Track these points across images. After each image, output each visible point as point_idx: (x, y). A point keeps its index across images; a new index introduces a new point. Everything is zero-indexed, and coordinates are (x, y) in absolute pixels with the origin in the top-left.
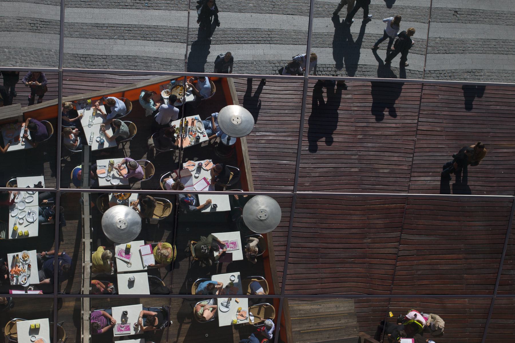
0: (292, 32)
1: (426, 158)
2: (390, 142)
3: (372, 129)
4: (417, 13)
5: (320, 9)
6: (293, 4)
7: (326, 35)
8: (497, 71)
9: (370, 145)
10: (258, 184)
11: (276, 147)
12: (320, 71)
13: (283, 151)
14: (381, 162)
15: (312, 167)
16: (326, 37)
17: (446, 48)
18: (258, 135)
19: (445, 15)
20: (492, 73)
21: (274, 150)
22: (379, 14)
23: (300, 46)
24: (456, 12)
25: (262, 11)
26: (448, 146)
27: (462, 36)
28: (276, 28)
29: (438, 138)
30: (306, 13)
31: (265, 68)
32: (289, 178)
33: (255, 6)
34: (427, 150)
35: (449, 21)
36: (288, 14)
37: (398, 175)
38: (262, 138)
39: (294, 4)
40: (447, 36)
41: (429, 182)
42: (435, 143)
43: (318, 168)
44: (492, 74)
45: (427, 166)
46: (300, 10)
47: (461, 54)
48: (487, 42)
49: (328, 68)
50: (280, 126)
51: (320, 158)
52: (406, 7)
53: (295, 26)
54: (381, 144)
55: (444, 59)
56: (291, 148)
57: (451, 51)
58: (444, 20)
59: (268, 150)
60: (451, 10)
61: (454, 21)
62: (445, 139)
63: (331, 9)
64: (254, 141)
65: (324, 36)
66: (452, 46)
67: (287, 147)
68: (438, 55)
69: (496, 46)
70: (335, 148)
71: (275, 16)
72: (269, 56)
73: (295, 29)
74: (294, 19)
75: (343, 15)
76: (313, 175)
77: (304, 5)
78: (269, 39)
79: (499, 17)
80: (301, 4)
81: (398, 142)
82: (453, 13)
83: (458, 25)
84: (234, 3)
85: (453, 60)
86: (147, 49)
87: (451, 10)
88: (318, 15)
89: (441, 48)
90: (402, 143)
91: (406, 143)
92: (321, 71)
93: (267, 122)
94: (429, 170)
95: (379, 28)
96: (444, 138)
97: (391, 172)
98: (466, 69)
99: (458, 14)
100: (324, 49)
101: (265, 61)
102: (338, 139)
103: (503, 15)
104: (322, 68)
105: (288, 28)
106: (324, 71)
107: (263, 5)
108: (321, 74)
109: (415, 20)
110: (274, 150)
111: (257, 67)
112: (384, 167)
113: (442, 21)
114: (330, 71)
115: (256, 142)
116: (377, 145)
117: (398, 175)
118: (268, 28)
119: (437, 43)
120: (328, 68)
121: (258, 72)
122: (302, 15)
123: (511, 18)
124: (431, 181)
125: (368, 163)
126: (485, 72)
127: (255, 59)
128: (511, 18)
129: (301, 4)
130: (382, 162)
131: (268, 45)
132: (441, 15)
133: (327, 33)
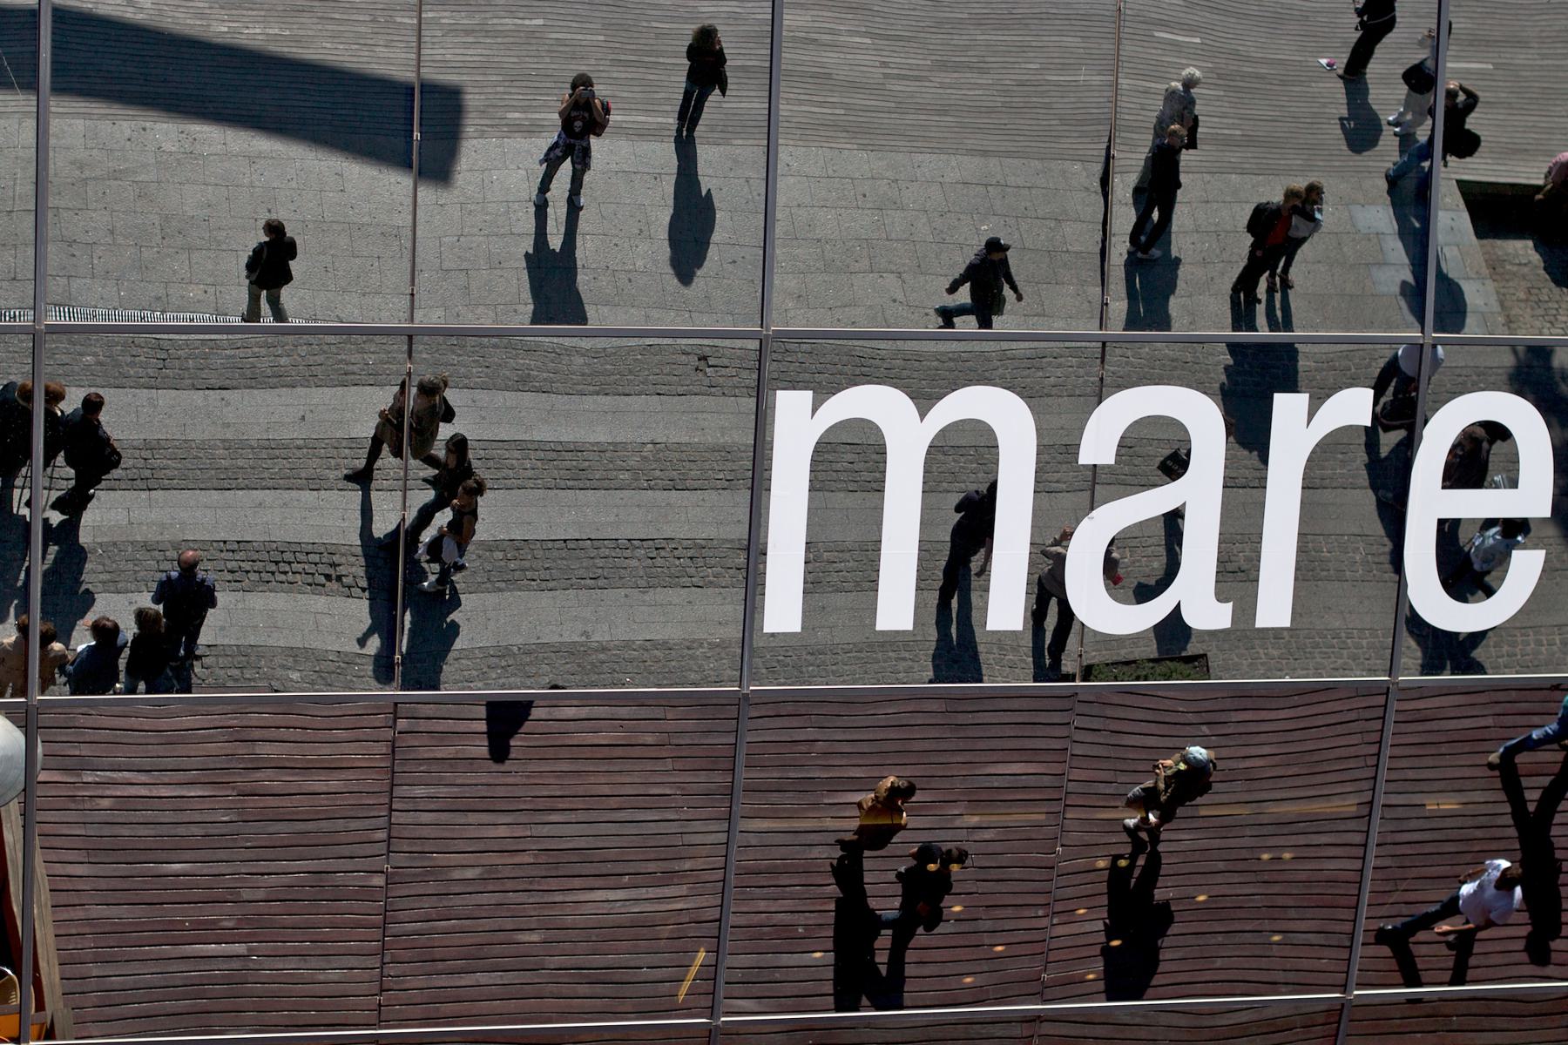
0: (219, 448)
1: (612, 828)
2: (484, 781)
3: (425, 739)
4: (608, 367)
5: (283, 361)
6: (228, 352)
7: (299, 448)
8: (857, 544)
9: (420, 791)
10: (87, 945)
11: (151, 820)
12: (284, 562)
13: (173, 832)
14: (455, 845)
15: (243, 871)
16: (299, 453)
17: (674, 473)
18: (90, 779)
19: (667, 369)
20: (842, 551)
21: (142, 831)
22: (485, 369)
23: (240, 492)
24: (704, 358)
25: (124, 380)
26: (683, 789)
27: (723, 436)
28: (169, 437)
29: (649, 765)
30: (266, 380)
31: (130, 566)
32: (186, 921)
33: (101, 364)
34: (613, 802)
35: (680, 390)
36: (208, 389)
37: (509, 885)
38: (99, 793)
39: (233, 352)
40: (677, 436)
41: (619, 904)
42: (639, 780)
43: (263, 874)
44: (841, 555)
45: (612, 854)
46: (248, 372)
47: (721, 491)
48: (828, 452)
49: (307, 554)
50: (161, 750)
51: (267, 844)
52: (566, 350)
53: (228, 425)
54: (456, 789)
55: (668, 504)
56: (200, 820)
57: (689, 483)
58: (667, 387)
59: (125, 831)
60: (689, 354)
61: (696, 389)
62: (671, 768)
63: (316, 357)
64: (74, 801)
65: (295, 451)
66: (692, 466)
67: (184, 820)
68: (649, 492)
69: (855, 466)
70: (318, 812)
71: (165, 397)
72: (145, 528)
73: (229, 436)
74: (228, 404)
75: (352, 377)
76: (246, 894)
77: (263, 351)
78: (147, 473)
79: (863, 369)
80: (257, 350)
81: (510, 780)
82: (694, 360)
83: (708, 402)
84: (10, 352)
85: (698, 509)
86: (838, 824)
87: (689, 354)
88: (278, 379)
89: (658, 473)
90: (524, 781)
91: (536, 782)
92: (290, 563)
93: (117, 736)
94: (620, 868)
95: (484, 418)
96: (669, 764)
97: (486, 876)
98: (739, 540)
99: (709, 366)
100: (294, 493)
101: (132, 543)
102: (327, 785)
103: (878, 362)
104: (292, 555)
105: (206, 436)
106: (298, 563)
107: (129, 359)
108: (287, 569)
109: (598, 388)
110: (142, 831)
111: (107, 562)
112: (465, 863)
113: (662, 389)
114: (316, 564)
115: (81, 807)
116: (443, 791)
117: (509, 885)
118: (144, 437)
119: (645, 459)
120: (307, 554)
121: (109, 577)
122: (252, 388)
123: (905, 373)
124: (627, 903)
125: (414, 849)
126: (819, 551)
127: (99, 540)
128: (905, 373)
129: (257, 350)
130: (461, 845)
131: (144, 495)
132: (658, 371)
133: (302, 442)
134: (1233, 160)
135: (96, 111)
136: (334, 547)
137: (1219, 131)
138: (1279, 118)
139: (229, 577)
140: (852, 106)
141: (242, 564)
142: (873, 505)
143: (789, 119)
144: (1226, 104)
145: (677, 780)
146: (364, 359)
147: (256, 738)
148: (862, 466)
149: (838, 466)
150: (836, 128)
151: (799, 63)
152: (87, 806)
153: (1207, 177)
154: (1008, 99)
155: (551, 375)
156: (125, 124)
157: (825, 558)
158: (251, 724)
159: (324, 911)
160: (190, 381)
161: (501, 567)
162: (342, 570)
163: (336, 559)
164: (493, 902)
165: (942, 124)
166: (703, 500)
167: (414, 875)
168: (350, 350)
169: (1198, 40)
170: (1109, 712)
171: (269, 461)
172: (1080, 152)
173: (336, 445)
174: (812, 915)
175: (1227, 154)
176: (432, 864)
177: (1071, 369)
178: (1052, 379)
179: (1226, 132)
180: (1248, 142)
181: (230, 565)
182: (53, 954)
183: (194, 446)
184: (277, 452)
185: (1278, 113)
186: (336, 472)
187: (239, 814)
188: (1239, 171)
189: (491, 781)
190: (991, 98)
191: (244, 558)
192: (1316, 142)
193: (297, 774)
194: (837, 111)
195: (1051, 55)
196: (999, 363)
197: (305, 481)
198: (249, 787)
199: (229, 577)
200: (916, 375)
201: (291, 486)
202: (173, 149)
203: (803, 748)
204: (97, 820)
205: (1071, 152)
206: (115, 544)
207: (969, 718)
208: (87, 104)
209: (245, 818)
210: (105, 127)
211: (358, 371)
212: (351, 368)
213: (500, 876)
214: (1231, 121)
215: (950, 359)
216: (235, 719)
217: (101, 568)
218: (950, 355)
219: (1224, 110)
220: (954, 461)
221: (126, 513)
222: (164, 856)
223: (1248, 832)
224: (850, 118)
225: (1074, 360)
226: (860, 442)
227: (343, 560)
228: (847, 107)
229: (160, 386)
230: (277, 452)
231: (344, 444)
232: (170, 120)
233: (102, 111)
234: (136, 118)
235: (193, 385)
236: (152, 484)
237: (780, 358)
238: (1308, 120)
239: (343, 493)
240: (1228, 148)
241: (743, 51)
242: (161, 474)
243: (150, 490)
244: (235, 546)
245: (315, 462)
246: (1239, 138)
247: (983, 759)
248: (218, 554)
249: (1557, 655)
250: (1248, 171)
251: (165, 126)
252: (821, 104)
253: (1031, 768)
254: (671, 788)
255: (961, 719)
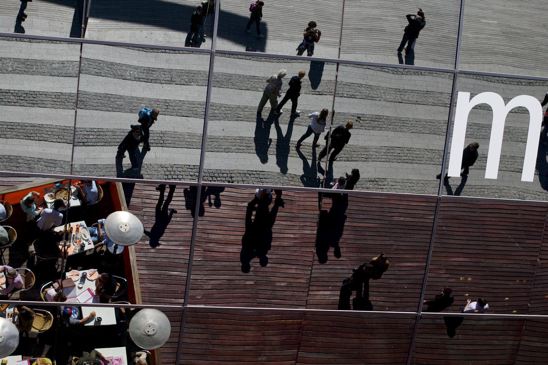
0: (186, 135)
5: (216, 111)
6: (188, 105)
13: (174, 261)
16: (221, 141)
17: (348, 155)
26: (349, 259)
30: (201, 116)
32: (179, 291)
36: (182, 116)
39: (189, 105)
41: (328, 296)
43: (211, 280)
44: (396, 183)
47: (363, 162)
49: (223, 174)
52: (306, 111)
53: (189, 128)
56: (183, 258)
57: (353, 159)
63: (228, 111)
65: (220, 140)
67: (178, 257)
69: (401, 155)
74: (189, 122)
75: (240, 118)
76: (205, 287)
78: (162, 142)
79: (404, 124)
81: (296, 254)
88: (214, 118)
90: (300, 254)
91: (305, 255)
92: (217, 177)
94: (328, 284)
101: (157, 164)
102: (233, 250)
103: (408, 122)
105: (182, 131)
106: (220, 177)
107: (156, 105)
111: (148, 171)
112: (281, 280)
114: (225, 177)
115: (145, 252)
120: (223, 174)
122: (196, 117)
123: (416, 125)
124: (331, 296)
126: (388, 182)
128: (416, 125)
129: (197, 105)
134: (510, 61)
135: (135, 27)
136: (232, 171)
137: (504, 51)
138: (525, 48)
139: (191, 178)
140: (392, 41)
141: (195, 173)
142: (406, 168)
143: (371, 45)
144: (506, 42)
145: (347, 255)
146: (244, 113)
147: (209, 233)
148: (402, 154)
149: (395, 154)
150: (386, 48)
151: (375, 26)
152: (146, 251)
153: (501, 66)
154: (440, 42)
155: (301, 120)
156: (145, 32)
157: (391, 184)
158: (207, 228)
159: (231, 292)
160: (175, 113)
161: (287, 182)
162: (234, 179)
163: (232, 175)
164: (290, 295)
165: (421, 48)
166: (357, 165)
167: (264, 283)
168: (239, 110)
169: (496, 22)
170: (486, 239)
171: (210, 143)
172: (468, 60)
173: (235, 138)
174: (391, 303)
175: (507, 59)
176: (270, 280)
177: (475, 130)
178: (469, 132)
179: (506, 51)
180: (515, 55)
181: (191, 173)
183: (178, 134)
184: (214, 140)
185: (524, 46)
186: (235, 147)
187: (204, 258)
188: (513, 66)
189: (290, 254)
190: (435, 41)
191: (196, 171)
192: (537, 58)
193: (222, 245)
194: (387, 42)
195: (452, 28)
196: (444, 124)
197: (224, 150)
198: (207, 248)
199: (191, 178)
200: (419, 126)
201: (218, 151)
202: (162, 40)
203: (389, 247)
204: (150, 256)
205: (465, 60)
206: (151, 165)
207: (446, 241)
208: (132, 25)
209: (206, 260)
211: (242, 117)
212: (240, 116)
213: (293, 286)
214: (508, 47)
215: (429, 122)
216: (201, 226)
217: (146, 173)
218: (429, 121)
219: (505, 44)
220: (431, 154)
221: (154, 154)
222: (171, 269)
223: (540, 286)
224: (391, 45)
225: (476, 127)
226: (402, 147)
227: (235, 175)
228: (391, 41)
229: (166, 114)
230: (214, 140)
231: (238, 138)
232: (161, 30)
233: (138, 27)
234: (149, 29)
235: (177, 115)
237: (378, 120)
238: (535, 50)
239: (237, 153)
240: (507, 57)
241: (360, 24)
242: (167, 142)
243: (163, 147)
244: (193, 167)
245: (228, 144)
246: (511, 54)
247: (451, 256)
248: (187, 169)
250: (516, 66)
252: (381, 40)
253: (466, 260)
254: (345, 258)
255: (443, 241)
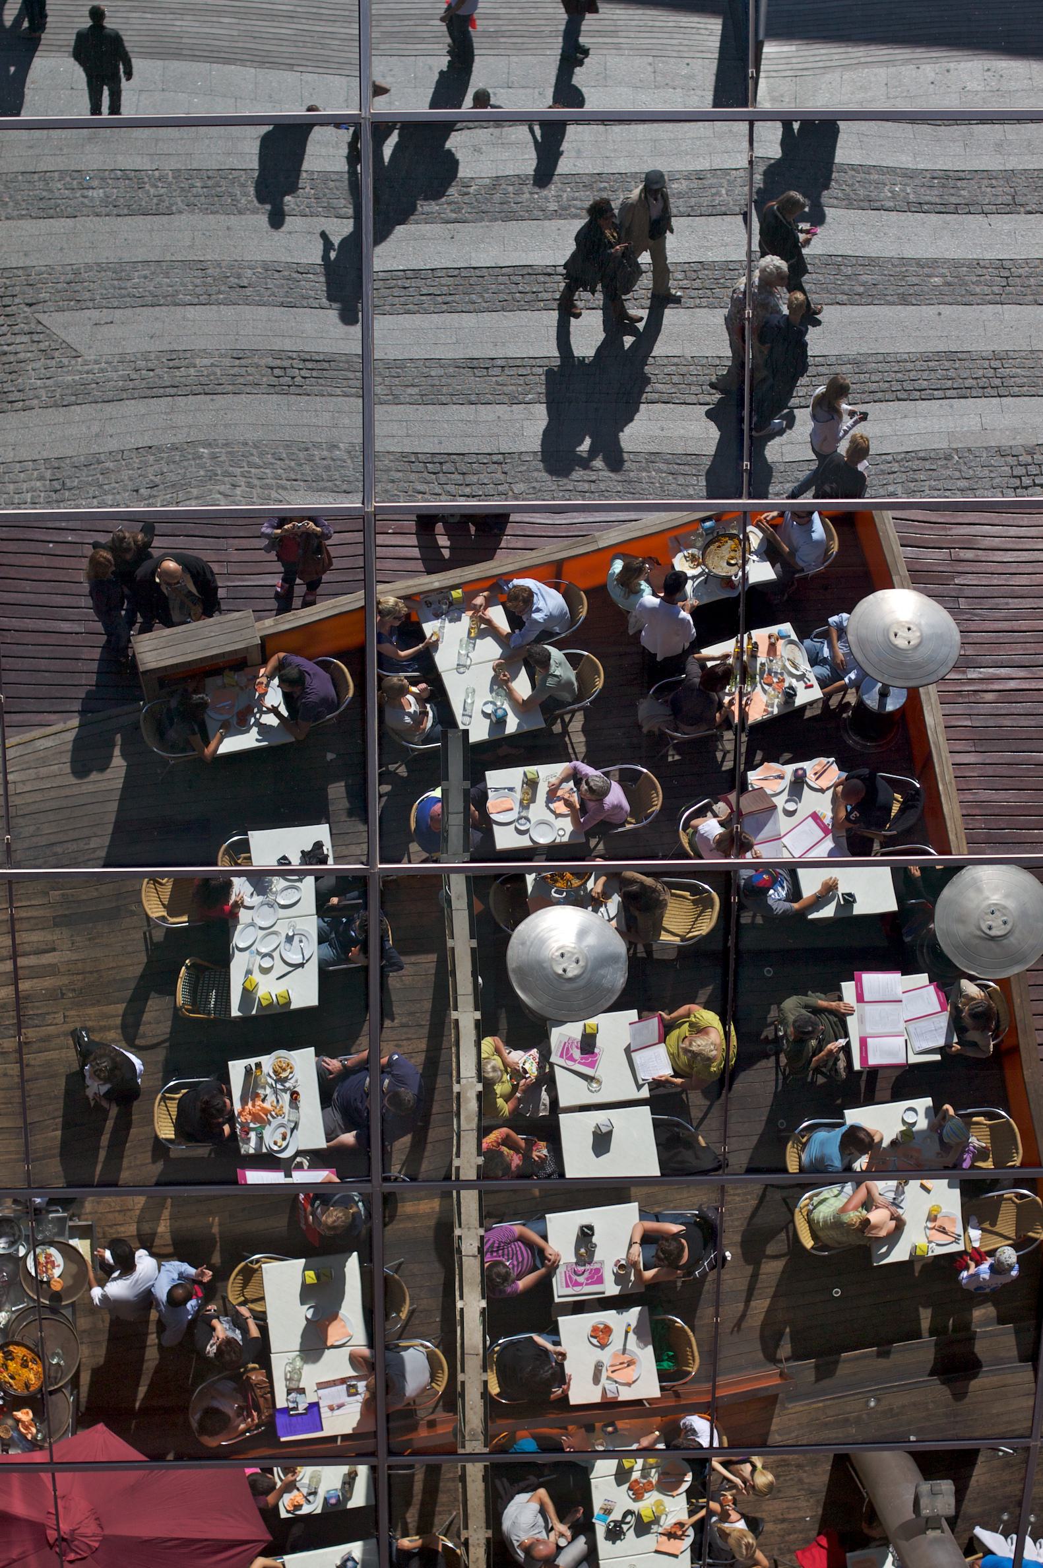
18: (974, 676)
31: (986, 472)
38: (984, 687)
64: (961, 696)
71: (1010, 312)
78: (997, 382)
101: (986, 448)
107: (975, 279)
111: (964, 468)
127: (954, 446)
182: (962, 834)
204: (982, 712)
206: (969, 450)
208: (891, 51)
210: (908, 71)
217: (957, 474)
233: (907, 56)
236: (1002, 391)
242: (1008, 382)
249: (972, 1264)
251: (970, 64)
